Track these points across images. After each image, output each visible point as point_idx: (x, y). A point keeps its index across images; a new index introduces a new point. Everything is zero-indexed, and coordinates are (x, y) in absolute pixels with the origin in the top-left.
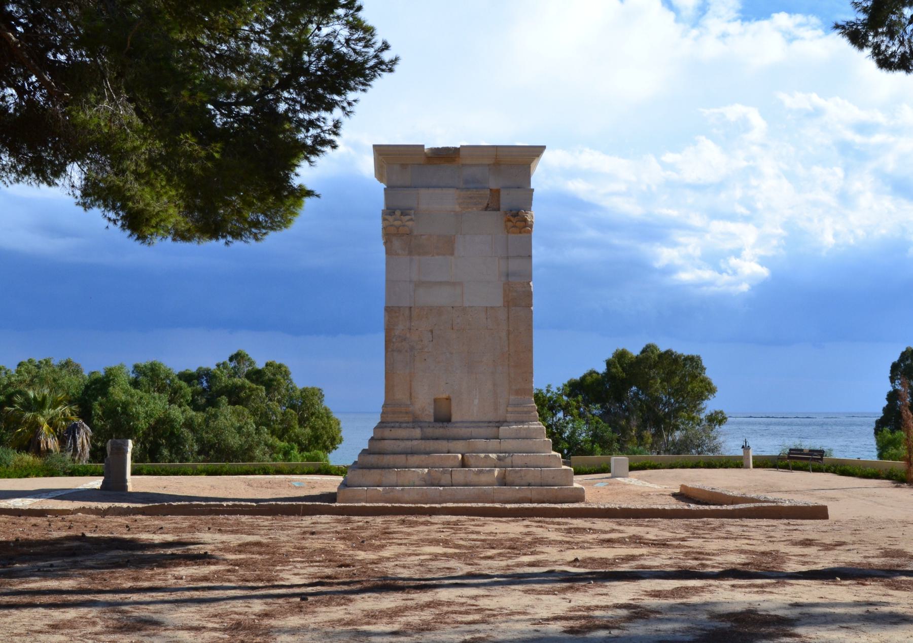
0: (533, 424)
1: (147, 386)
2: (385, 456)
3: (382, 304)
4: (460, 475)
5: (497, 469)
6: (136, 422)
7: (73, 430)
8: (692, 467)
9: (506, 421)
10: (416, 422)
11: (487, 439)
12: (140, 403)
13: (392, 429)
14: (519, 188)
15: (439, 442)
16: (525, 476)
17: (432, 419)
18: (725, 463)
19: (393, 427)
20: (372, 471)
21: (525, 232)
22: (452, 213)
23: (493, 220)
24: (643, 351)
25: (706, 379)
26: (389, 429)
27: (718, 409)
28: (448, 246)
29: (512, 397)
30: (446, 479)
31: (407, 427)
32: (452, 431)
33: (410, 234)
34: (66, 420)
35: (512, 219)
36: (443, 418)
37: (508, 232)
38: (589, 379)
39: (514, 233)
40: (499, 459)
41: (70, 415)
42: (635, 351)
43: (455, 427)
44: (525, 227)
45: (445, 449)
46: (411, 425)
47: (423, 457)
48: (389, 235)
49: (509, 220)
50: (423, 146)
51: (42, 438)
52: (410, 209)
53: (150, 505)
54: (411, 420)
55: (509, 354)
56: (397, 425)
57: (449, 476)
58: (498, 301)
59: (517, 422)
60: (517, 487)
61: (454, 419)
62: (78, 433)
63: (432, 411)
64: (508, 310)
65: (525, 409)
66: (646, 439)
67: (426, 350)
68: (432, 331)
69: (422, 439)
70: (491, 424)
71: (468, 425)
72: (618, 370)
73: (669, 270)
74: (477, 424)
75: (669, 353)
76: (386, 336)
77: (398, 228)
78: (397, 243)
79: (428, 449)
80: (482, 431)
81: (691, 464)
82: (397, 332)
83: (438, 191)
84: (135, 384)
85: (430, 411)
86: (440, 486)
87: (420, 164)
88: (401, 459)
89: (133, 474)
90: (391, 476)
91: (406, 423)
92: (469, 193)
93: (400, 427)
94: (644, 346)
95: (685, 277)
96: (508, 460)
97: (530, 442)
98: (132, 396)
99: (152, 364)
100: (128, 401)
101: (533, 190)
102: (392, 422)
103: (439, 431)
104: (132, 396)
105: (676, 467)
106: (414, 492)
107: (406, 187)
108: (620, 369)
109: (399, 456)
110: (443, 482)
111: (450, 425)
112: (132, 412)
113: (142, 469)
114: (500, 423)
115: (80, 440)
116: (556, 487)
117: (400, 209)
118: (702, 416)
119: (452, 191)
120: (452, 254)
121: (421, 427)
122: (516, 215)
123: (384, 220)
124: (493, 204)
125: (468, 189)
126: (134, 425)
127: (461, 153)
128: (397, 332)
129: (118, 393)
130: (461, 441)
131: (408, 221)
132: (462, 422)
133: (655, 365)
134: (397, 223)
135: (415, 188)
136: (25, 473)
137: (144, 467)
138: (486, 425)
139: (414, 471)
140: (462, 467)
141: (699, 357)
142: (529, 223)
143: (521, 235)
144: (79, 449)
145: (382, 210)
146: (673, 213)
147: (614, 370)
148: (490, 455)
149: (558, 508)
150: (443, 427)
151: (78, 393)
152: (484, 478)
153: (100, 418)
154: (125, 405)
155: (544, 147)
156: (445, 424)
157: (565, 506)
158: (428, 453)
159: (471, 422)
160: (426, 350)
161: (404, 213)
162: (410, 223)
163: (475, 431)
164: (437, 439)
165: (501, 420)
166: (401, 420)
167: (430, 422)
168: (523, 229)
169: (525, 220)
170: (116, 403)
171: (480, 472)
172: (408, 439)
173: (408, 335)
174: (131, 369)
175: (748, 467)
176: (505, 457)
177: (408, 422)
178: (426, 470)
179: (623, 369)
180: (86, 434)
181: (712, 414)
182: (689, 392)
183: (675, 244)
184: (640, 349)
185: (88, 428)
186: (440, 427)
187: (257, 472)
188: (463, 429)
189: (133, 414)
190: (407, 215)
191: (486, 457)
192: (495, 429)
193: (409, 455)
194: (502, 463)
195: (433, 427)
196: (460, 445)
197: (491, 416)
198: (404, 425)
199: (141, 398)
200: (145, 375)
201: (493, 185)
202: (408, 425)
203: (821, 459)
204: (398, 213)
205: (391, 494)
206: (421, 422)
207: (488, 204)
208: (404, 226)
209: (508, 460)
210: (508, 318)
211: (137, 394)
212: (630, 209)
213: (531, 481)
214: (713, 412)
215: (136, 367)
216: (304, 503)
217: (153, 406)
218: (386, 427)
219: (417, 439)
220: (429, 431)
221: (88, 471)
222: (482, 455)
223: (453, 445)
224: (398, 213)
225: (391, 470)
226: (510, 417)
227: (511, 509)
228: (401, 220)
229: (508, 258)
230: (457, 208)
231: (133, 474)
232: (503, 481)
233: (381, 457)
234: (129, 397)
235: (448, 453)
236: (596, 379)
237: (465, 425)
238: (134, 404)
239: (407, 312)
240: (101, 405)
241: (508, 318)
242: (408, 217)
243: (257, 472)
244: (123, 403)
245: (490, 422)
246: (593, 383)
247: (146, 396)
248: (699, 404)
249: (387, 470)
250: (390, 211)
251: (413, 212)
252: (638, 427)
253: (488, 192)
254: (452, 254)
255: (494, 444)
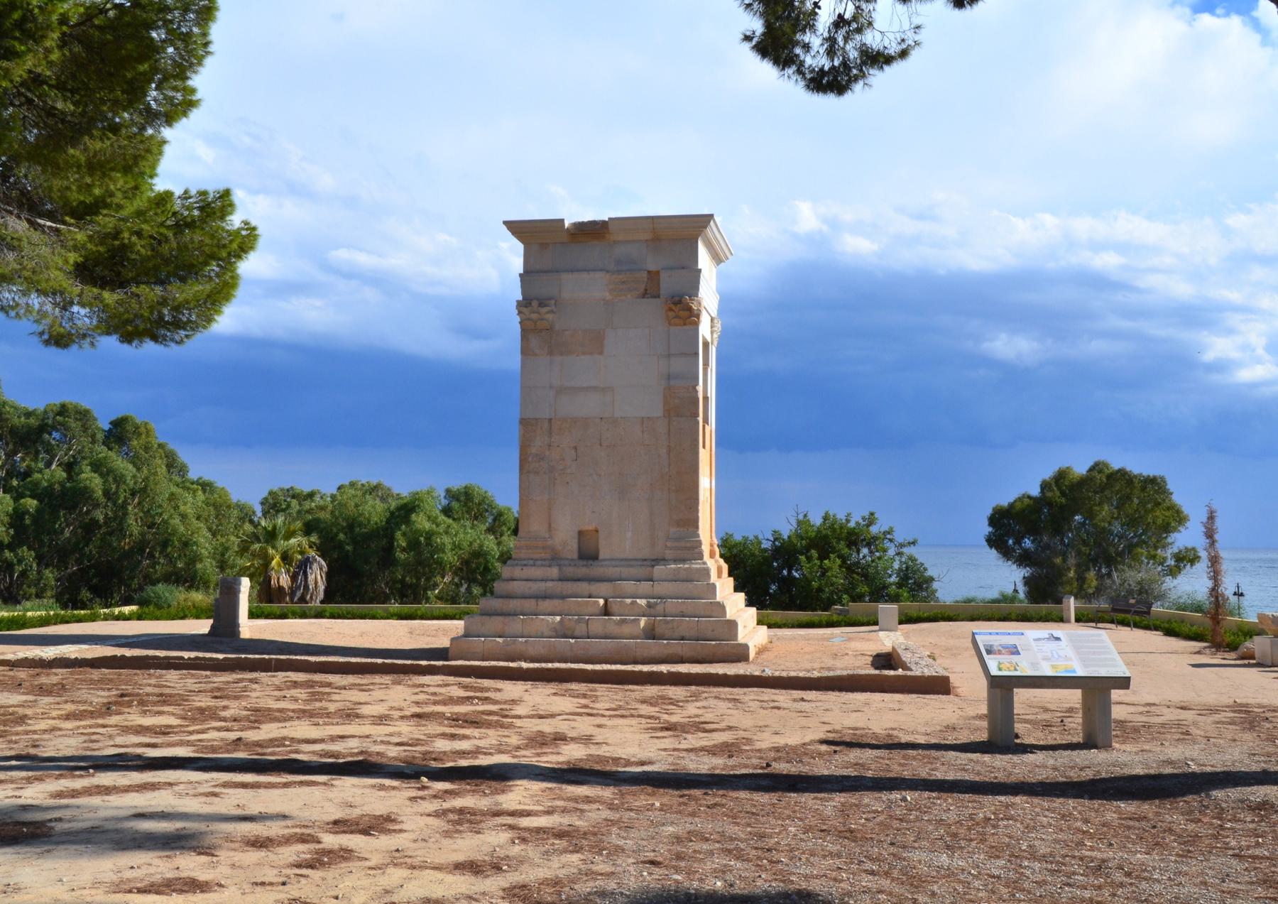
0: (697, 564)
1: (460, 512)
2: (511, 600)
3: (515, 413)
4: (598, 624)
5: (643, 618)
6: (441, 555)
7: (305, 564)
8: (1000, 620)
9: (664, 560)
10: (555, 559)
11: (639, 581)
12: (447, 533)
13: (524, 568)
14: (683, 268)
15: (579, 584)
16: (678, 627)
17: (575, 556)
18: (1046, 616)
19: (525, 565)
20: (494, 618)
21: (690, 324)
22: (602, 302)
23: (652, 311)
24: (1091, 470)
25: (1175, 505)
26: (520, 568)
27: (1190, 546)
28: (596, 342)
29: (673, 530)
30: (581, 629)
31: (542, 565)
32: (597, 570)
33: (550, 329)
34: (302, 553)
35: (674, 308)
36: (588, 554)
37: (670, 324)
38: (1019, 506)
39: (676, 325)
40: (649, 605)
41: (307, 547)
42: (1080, 468)
43: (602, 566)
44: (690, 317)
45: (586, 593)
46: (547, 563)
47: (556, 602)
48: (529, 330)
49: (671, 310)
50: (562, 221)
51: (273, 574)
52: (550, 299)
53: (243, 656)
54: (548, 556)
55: (670, 476)
56: (531, 562)
57: (584, 625)
58: (658, 412)
59: (676, 561)
60: (665, 642)
61: (601, 556)
62: (311, 568)
63: (575, 546)
64: (669, 422)
65: (688, 545)
66: (1089, 582)
67: (569, 471)
68: (575, 448)
69: (560, 580)
70: (645, 563)
71: (617, 563)
72: (1055, 494)
73: (1220, 366)
74: (627, 562)
75: (1122, 473)
76: (521, 455)
77: (535, 322)
78: (534, 341)
79: (564, 593)
80: (634, 571)
81: (997, 617)
82: (534, 451)
83: (584, 275)
84: (447, 511)
85: (574, 545)
86: (573, 638)
87: (563, 243)
88: (529, 604)
89: (252, 615)
90: (516, 625)
91: (541, 560)
92: (621, 277)
93: (534, 565)
94: (1092, 464)
95: (1246, 375)
96: (660, 608)
97: (690, 585)
98: (438, 525)
99: (466, 487)
100: (432, 530)
101: (700, 270)
102: (525, 560)
103: (582, 571)
104: (438, 525)
105: (978, 619)
106: (538, 645)
107: (545, 272)
108: (1058, 493)
109: (529, 600)
110: (577, 633)
111: (596, 563)
112: (436, 542)
113: (325, 611)
114: (657, 561)
115: (313, 576)
116: (714, 643)
117: (538, 300)
118: (1169, 553)
119: (599, 275)
120: (601, 353)
121: (559, 565)
122: (680, 302)
123: (520, 313)
124: (651, 289)
125: (619, 272)
126: (438, 558)
127: (610, 227)
128: (534, 451)
129: (421, 522)
130: (605, 583)
131: (547, 313)
132: (612, 560)
133: (1102, 489)
134: (534, 316)
135: (557, 272)
136: (182, 614)
137: (328, 609)
138: (639, 563)
139: (543, 619)
140: (605, 615)
141: (1162, 478)
142: (696, 312)
143: (685, 327)
144: (311, 587)
145: (518, 301)
146: (1234, 296)
147: (1049, 494)
148: (638, 600)
149: (587, 670)
150: (586, 566)
151: (381, 521)
152: (627, 629)
153: (404, 550)
154: (429, 535)
155: (505, 223)
156: (591, 562)
157: (645, 668)
158: (563, 597)
159: (622, 560)
160: (569, 471)
161: (542, 304)
162: (550, 317)
163: (626, 571)
164: (579, 580)
165: (660, 558)
166: (535, 556)
167: (572, 560)
168: (689, 320)
169: (690, 309)
170: (418, 532)
171: (623, 621)
172: (542, 580)
173: (547, 453)
174: (443, 494)
175: (1068, 621)
176: (656, 604)
177: (545, 560)
178: (558, 618)
179: (1063, 494)
180: (321, 569)
181: (1180, 551)
182: (1149, 523)
183: (1230, 332)
184: (1087, 468)
185: (323, 563)
186: (583, 566)
187: (458, 617)
188: (611, 569)
189: (437, 545)
190: (546, 306)
191: (633, 603)
192: (650, 569)
193: (540, 600)
194: (652, 611)
195: (575, 565)
196: (604, 588)
197: (646, 553)
198: (539, 563)
199: (449, 527)
200: (458, 500)
201: (652, 267)
202: (544, 563)
203: (1148, 613)
204: (535, 304)
205: (513, 646)
206: (562, 559)
207: (646, 290)
208: (542, 319)
209: (660, 608)
210: (669, 431)
211: (445, 523)
212: (1182, 290)
213: (687, 635)
214: (1182, 548)
215: (448, 491)
216: (278, 657)
217: (462, 536)
218: (517, 565)
219: (553, 580)
220: (570, 571)
221: (263, 612)
222: (629, 601)
223: (594, 588)
224: (535, 304)
225: (515, 617)
226: (669, 554)
227: (528, 670)
228: (539, 313)
229: (669, 356)
230: (608, 296)
231: (252, 615)
232: (651, 634)
233: (506, 601)
234: (434, 526)
235: (589, 597)
236: (1028, 505)
237: (614, 563)
238: (440, 533)
239: (546, 425)
240: (404, 534)
241: (669, 431)
242: (546, 309)
243: (458, 617)
244: (427, 533)
245: (645, 560)
246: (1023, 510)
247: (454, 525)
248: (1166, 537)
249: (511, 618)
250: (523, 305)
251: (553, 302)
252: (1078, 566)
253: (645, 275)
254: (601, 353)
255: (645, 587)
